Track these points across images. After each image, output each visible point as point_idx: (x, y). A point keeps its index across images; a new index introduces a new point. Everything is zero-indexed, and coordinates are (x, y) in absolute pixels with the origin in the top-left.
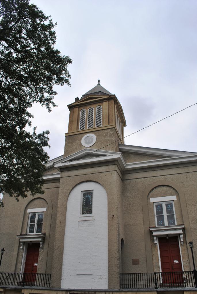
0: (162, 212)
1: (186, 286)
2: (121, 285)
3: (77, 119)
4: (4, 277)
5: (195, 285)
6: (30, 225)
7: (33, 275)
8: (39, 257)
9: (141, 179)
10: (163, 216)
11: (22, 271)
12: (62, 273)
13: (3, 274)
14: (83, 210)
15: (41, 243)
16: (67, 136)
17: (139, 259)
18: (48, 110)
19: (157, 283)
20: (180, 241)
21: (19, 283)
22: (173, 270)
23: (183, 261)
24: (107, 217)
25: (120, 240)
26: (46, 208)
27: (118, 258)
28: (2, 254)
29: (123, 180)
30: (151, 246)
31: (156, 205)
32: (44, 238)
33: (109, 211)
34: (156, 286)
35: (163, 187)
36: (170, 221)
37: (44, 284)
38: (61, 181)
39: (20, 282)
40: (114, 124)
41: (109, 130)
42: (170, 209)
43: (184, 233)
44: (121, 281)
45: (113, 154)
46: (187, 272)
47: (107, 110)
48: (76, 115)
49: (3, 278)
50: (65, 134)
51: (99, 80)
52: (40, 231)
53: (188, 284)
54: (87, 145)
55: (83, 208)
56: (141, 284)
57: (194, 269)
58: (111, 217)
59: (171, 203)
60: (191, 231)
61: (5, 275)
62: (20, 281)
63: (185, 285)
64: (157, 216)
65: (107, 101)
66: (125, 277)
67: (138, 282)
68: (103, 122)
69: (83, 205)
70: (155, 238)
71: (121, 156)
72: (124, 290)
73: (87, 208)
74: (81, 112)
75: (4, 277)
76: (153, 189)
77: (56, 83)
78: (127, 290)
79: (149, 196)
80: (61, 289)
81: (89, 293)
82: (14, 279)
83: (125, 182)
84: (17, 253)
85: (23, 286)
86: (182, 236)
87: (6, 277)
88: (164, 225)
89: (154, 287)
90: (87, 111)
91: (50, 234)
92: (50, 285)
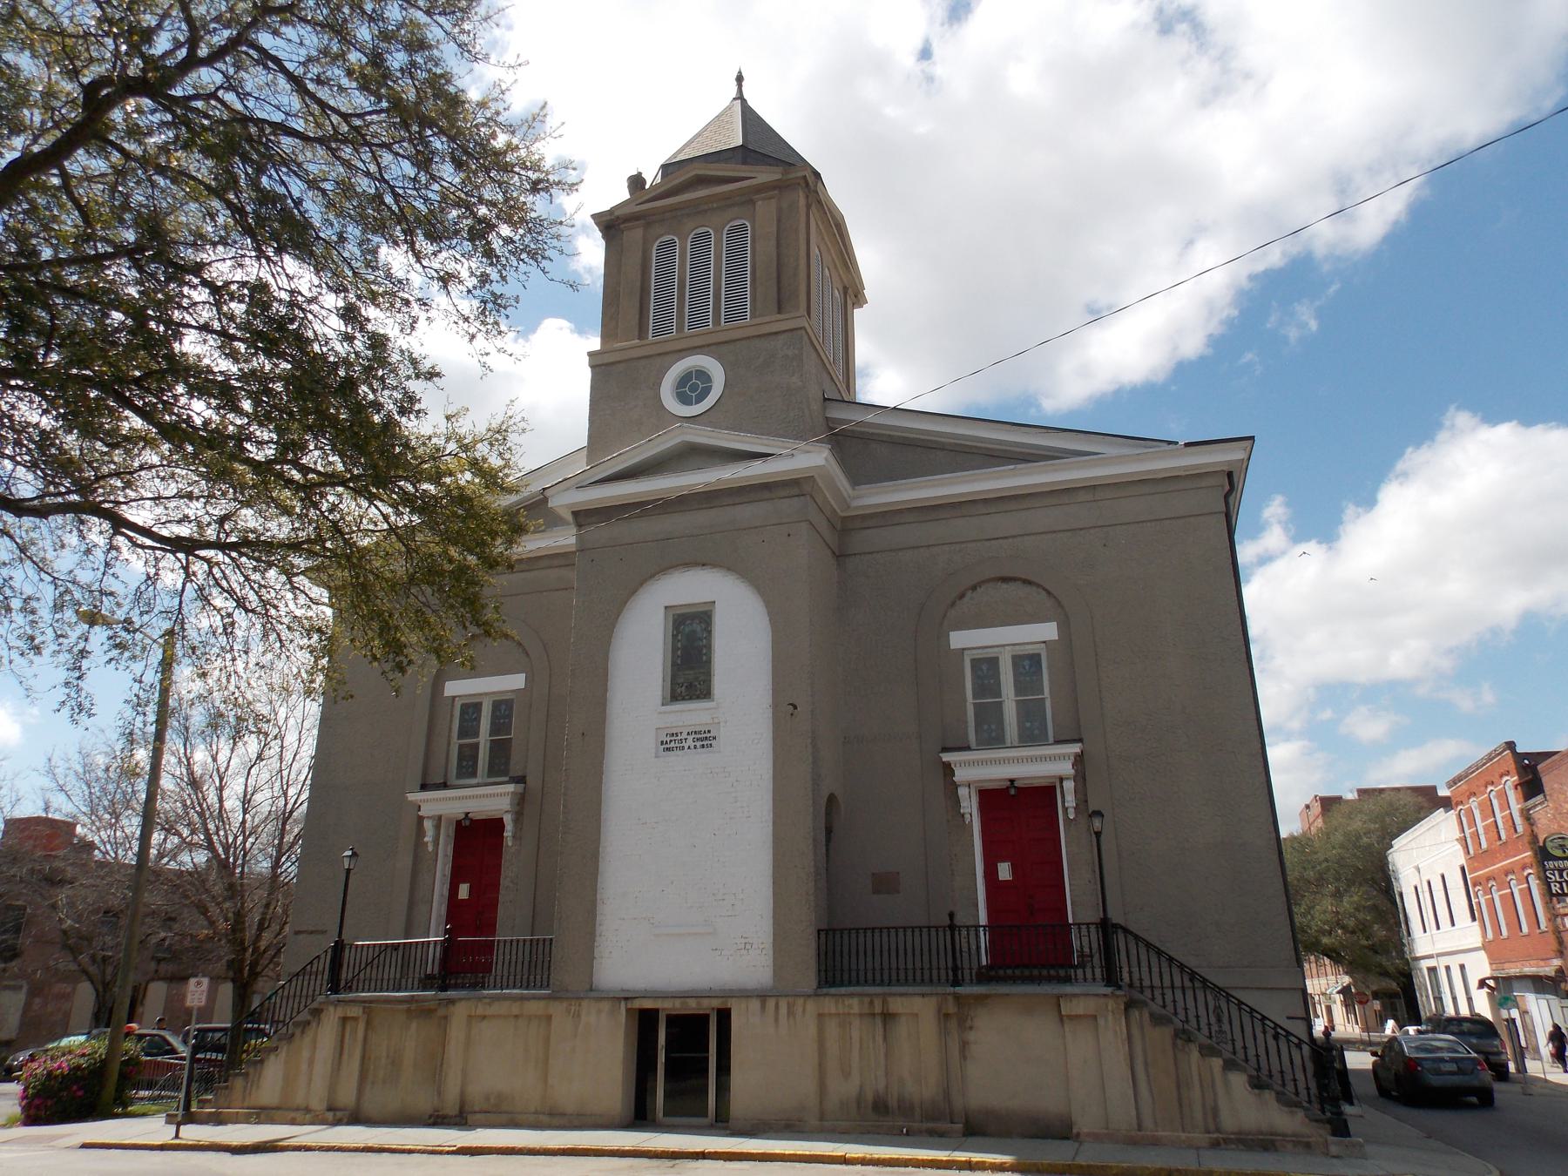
1: (1076, 979)
2: (823, 973)
10: (1001, 703)
12: (597, 934)
14: (674, 683)
16: (597, 366)
19: (960, 966)
26: (523, 676)
31: (973, 661)
33: (776, 692)
34: (955, 975)
35: (1005, 586)
37: (525, 977)
39: (428, 977)
40: (803, 311)
44: (823, 957)
46: (1084, 927)
47: (773, 242)
49: (357, 965)
50: (591, 354)
51: (740, 72)
54: (685, 407)
58: (785, 710)
59: (1036, 652)
62: (429, 971)
63: (1076, 975)
64: (974, 704)
68: (754, 300)
70: (963, 792)
71: (826, 459)
72: (833, 990)
74: (654, 252)
84: (410, 863)
87: (369, 968)
88: (1004, 743)
89: (947, 980)
90: (683, 249)
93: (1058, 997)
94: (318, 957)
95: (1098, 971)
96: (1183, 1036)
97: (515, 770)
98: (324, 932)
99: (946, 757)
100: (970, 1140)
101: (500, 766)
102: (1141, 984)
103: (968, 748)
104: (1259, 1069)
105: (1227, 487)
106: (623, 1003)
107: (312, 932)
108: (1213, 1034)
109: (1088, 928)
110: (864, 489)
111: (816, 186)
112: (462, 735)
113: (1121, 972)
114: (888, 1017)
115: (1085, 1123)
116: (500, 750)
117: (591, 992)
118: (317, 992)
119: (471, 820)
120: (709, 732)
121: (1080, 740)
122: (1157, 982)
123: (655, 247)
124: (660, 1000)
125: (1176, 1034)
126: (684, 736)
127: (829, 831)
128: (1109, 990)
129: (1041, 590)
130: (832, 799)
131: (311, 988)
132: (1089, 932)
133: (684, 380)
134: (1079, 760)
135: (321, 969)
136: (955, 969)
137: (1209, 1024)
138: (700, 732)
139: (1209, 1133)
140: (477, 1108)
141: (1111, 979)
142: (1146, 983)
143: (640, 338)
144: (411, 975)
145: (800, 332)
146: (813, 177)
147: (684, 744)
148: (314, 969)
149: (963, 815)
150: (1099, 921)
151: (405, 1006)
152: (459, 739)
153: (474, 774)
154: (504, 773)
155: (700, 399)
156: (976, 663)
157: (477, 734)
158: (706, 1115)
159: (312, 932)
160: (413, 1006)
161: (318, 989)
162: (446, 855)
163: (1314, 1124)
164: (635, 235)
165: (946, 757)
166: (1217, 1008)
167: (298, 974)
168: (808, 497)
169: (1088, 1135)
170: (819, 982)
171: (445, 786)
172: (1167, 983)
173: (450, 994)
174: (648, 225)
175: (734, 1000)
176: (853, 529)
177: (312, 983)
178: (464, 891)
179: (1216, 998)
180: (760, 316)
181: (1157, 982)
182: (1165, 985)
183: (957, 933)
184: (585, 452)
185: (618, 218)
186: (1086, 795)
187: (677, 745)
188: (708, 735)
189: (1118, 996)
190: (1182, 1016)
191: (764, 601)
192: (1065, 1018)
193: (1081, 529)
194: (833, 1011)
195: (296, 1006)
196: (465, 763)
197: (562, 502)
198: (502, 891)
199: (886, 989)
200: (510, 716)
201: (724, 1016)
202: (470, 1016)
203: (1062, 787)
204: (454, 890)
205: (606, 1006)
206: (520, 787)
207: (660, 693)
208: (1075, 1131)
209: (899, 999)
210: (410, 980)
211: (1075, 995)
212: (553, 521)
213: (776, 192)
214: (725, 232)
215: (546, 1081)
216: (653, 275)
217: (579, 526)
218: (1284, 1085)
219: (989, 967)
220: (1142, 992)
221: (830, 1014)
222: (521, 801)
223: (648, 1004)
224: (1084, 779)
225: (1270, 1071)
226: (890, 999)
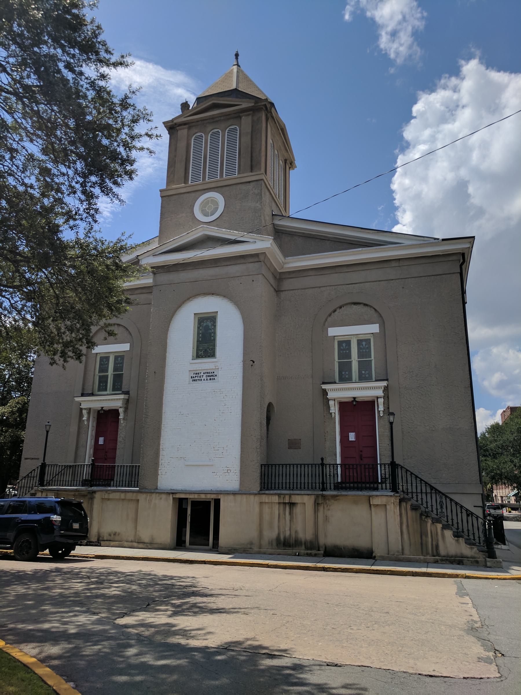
0: (349, 356)
3: (184, 157)
4: (55, 471)
5: (390, 487)
8: (119, 437)
9: (314, 289)
10: (351, 362)
11: (88, 461)
12: (160, 464)
13: (53, 467)
15: (121, 411)
18: (63, 369)
20: (378, 410)
22: (361, 460)
23: (380, 445)
24: (242, 363)
25: (266, 406)
27: (259, 437)
28: (47, 432)
29: (278, 291)
31: (338, 342)
33: (246, 353)
35: (355, 307)
36: (363, 372)
39: (86, 480)
41: (251, 186)
42: (364, 350)
44: (263, 477)
45: (256, 241)
48: (182, 145)
50: (161, 191)
52: (119, 387)
56: (297, 483)
57: (391, 460)
60: (400, 392)
61: (55, 469)
65: (249, 115)
67: (295, 479)
69: (197, 341)
70: (331, 403)
71: (271, 244)
72: (267, 492)
74: (193, 141)
75: (55, 471)
78: (272, 492)
79: (327, 323)
80: (157, 491)
81: (206, 496)
82: (74, 474)
83: (283, 295)
86: (381, 401)
87: (57, 473)
88: (352, 381)
89: (319, 488)
92: (138, 483)
93: (370, 497)
94: (34, 470)
95: (388, 485)
96: (425, 515)
97: (125, 388)
98: (38, 459)
99: (324, 387)
100: (327, 559)
101: (117, 387)
102: (407, 491)
103: (335, 383)
104: (458, 529)
105: (462, 261)
106: (171, 495)
107: (32, 459)
108: (438, 513)
110: (289, 259)
111: (271, 109)
112: (100, 372)
113: (398, 485)
114: (292, 505)
115: (378, 552)
116: (118, 378)
117: (155, 491)
118: (33, 486)
119: (104, 410)
120: (214, 372)
121: (387, 380)
122: (414, 490)
123: (193, 139)
124: (188, 494)
125: (421, 515)
126: (202, 374)
127: (268, 419)
128: (392, 494)
129: (372, 309)
130: (270, 405)
131: (31, 483)
133: (205, 203)
134: (386, 389)
135: (35, 475)
136: (323, 483)
137: (437, 509)
138: (209, 373)
139: (434, 556)
140: (105, 539)
141: (394, 489)
142: (410, 490)
143: (185, 183)
145: (261, 182)
146: (269, 105)
147: (202, 378)
148: (33, 475)
149: (331, 414)
150: (389, 462)
151: (73, 493)
152: (99, 373)
153: (106, 390)
154: (120, 389)
155: (212, 214)
156: (340, 343)
157: (107, 371)
158: (208, 545)
159: (32, 459)
160: (77, 493)
161: (34, 484)
162: (93, 426)
163: (482, 553)
164: (183, 132)
165: (324, 387)
166: (441, 502)
167: (25, 477)
168: (262, 263)
169: (380, 556)
170: (261, 488)
171: (92, 394)
172: (419, 491)
173: (94, 488)
174: (189, 128)
175: (222, 495)
176: (285, 278)
177: (32, 481)
178: (101, 441)
179: (441, 498)
180: (243, 173)
181: (414, 490)
182: (418, 491)
183: (324, 467)
184: (158, 239)
185: (176, 124)
186: (389, 405)
187: (199, 378)
188: (213, 374)
189: (396, 496)
190: (425, 505)
191: (240, 312)
192: (372, 506)
193: (392, 280)
194: (267, 501)
195: (24, 491)
196: (102, 384)
197: (147, 261)
198: (118, 444)
199: (292, 492)
200: (122, 363)
201: (217, 502)
202: (102, 499)
203: (378, 401)
204: (97, 441)
205: (164, 496)
206: (126, 397)
207: (191, 354)
208: (374, 555)
209: (297, 496)
211: (377, 496)
212: (142, 270)
213: (251, 112)
214: (227, 131)
215: (136, 529)
217: (154, 273)
218: (469, 536)
219: (342, 483)
220: (407, 495)
221: (265, 503)
222: (127, 402)
223: (183, 496)
224: (388, 397)
225: (463, 529)
226: (293, 496)
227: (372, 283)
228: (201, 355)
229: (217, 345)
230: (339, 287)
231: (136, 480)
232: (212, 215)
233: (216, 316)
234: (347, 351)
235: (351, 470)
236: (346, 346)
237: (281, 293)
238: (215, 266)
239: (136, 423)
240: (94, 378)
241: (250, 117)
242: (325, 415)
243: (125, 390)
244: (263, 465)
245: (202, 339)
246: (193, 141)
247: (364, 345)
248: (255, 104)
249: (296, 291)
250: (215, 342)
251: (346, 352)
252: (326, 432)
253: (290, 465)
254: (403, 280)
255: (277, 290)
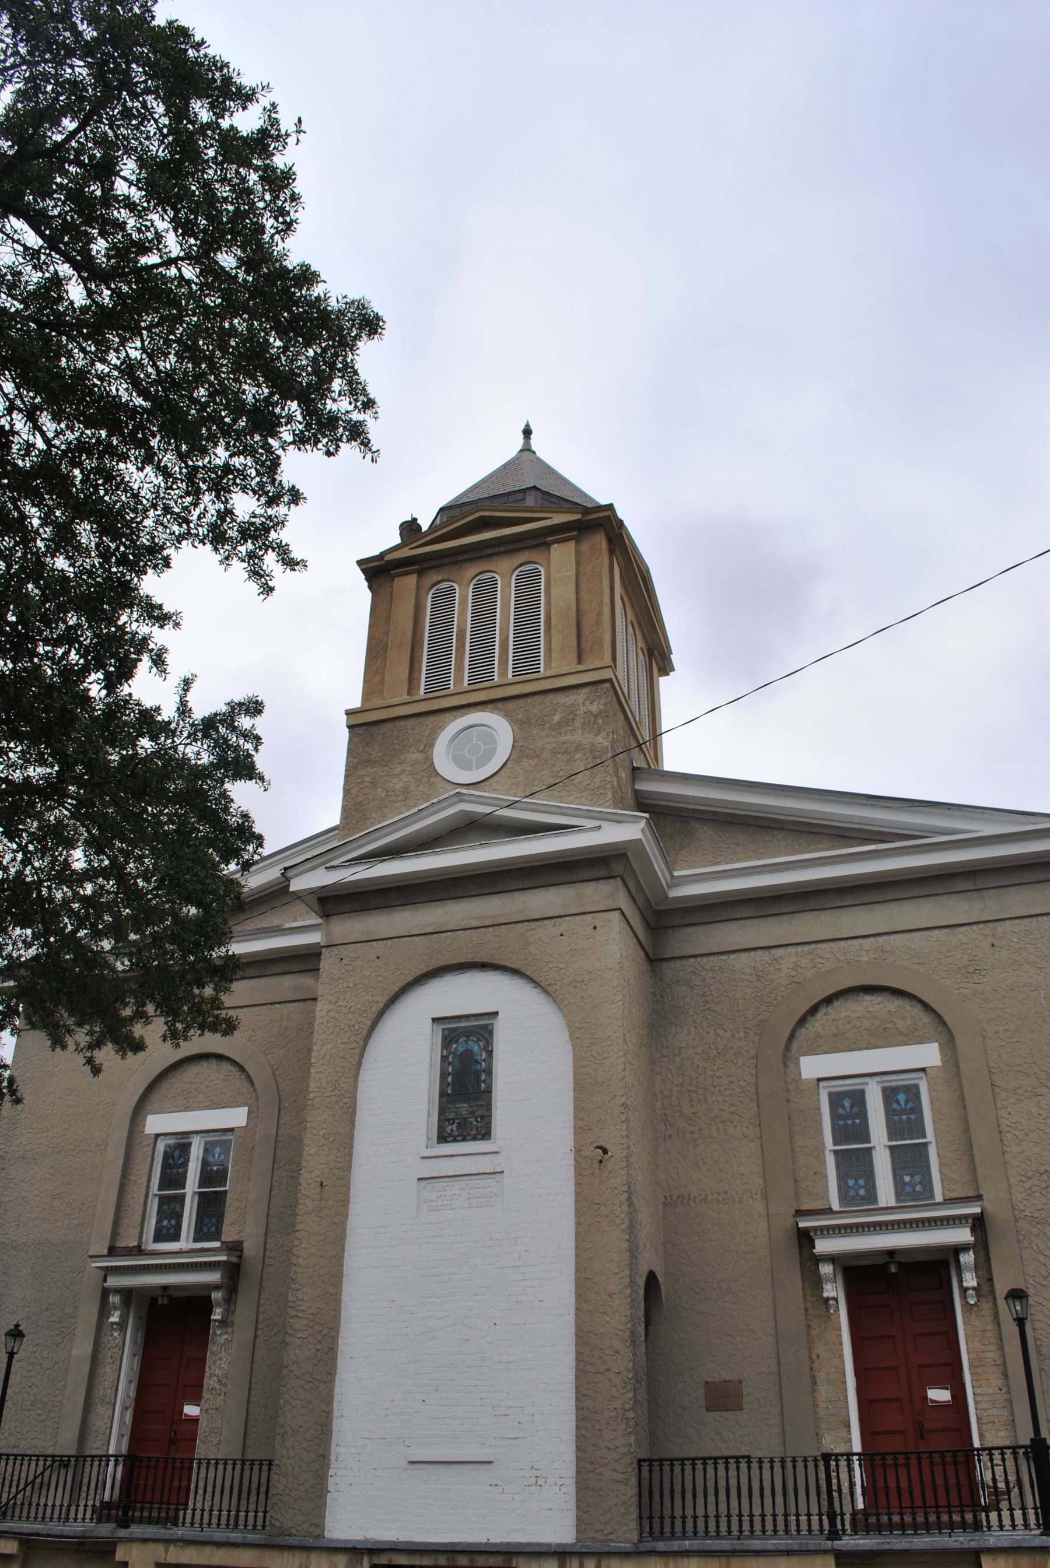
3: (410, 635)
4: (23, 1475)
5: (1037, 1519)
6: (163, 1200)
7: (178, 1465)
10: (869, 1150)
11: (116, 1444)
14: (443, 1119)
15: (216, 1296)
17: (740, 1382)
21: (103, 1512)
22: (922, 1438)
23: (978, 1391)
25: (642, 1281)
28: (11, 1355)
30: (807, 1310)
31: (830, 1095)
32: (234, 1272)
33: (580, 1130)
34: (832, 1523)
35: (868, 998)
36: (907, 1179)
38: (327, 961)
39: (107, 1506)
40: (607, 660)
42: (904, 1117)
43: (982, 1245)
46: (996, 1452)
47: (572, 586)
48: (403, 613)
49: (15, 1483)
50: (349, 713)
51: (528, 425)
52: (213, 1229)
53: (1000, 1516)
55: (442, 1111)
56: (740, 1516)
63: (988, 1521)
64: (836, 1152)
65: (568, 540)
66: (666, 1479)
67: (734, 1503)
68: (549, 650)
69: (441, 1096)
70: (826, 1269)
71: (642, 830)
72: (661, 1546)
73: (464, 1108)
74: (429, 600)
75: (23, 1475)
76: (814, 1010)
77: (300, 441)
78: (675, 1545)
79: (795, 1046)
81: (472, 1561)
82: (76, 1487)
83: (669, 970)
85: (125, 1524)
86: (967, 1259)
87: (29, 1488)
89: (821, 1530)
91: (265, 1249)
109: (1003, 1454)
121: (979, 1197)
129: (915, 1003)
132: (1003, 1460)
144: (82, 1503)
150: (1027, 1442)
155: (481, 763)
157: (182, 1185)
170: (641, 1533)
174: (421, 573)
210: (81, 1509)
216: (427, 624)
227: (908, 936)
228: (450, 1135)
229: (499, 1105)
230: (820, 946)
231: (261, 1509)
232: (479, 766)
233: (493, 1024)
234: (857, 1121)
235: (891, 1472)
236: (852, 1106)
237: (664, 965)
238: (491, 891)
239: (259, 1333)
240: (145, 1204)
241: (572, 544)
242: (809, 1305)
243: (230, 1239)
244: (644, 1460)
245: (453, 1090)
246: (429, 600)
247: (902, 1103)
248: (583, 515)
249: (705, 959)
250: (490, 1097)
251: (909, 1119)
252: (814, 1357)
253: (715, 1459)
254: (991, 925)
255: (652, 957)
